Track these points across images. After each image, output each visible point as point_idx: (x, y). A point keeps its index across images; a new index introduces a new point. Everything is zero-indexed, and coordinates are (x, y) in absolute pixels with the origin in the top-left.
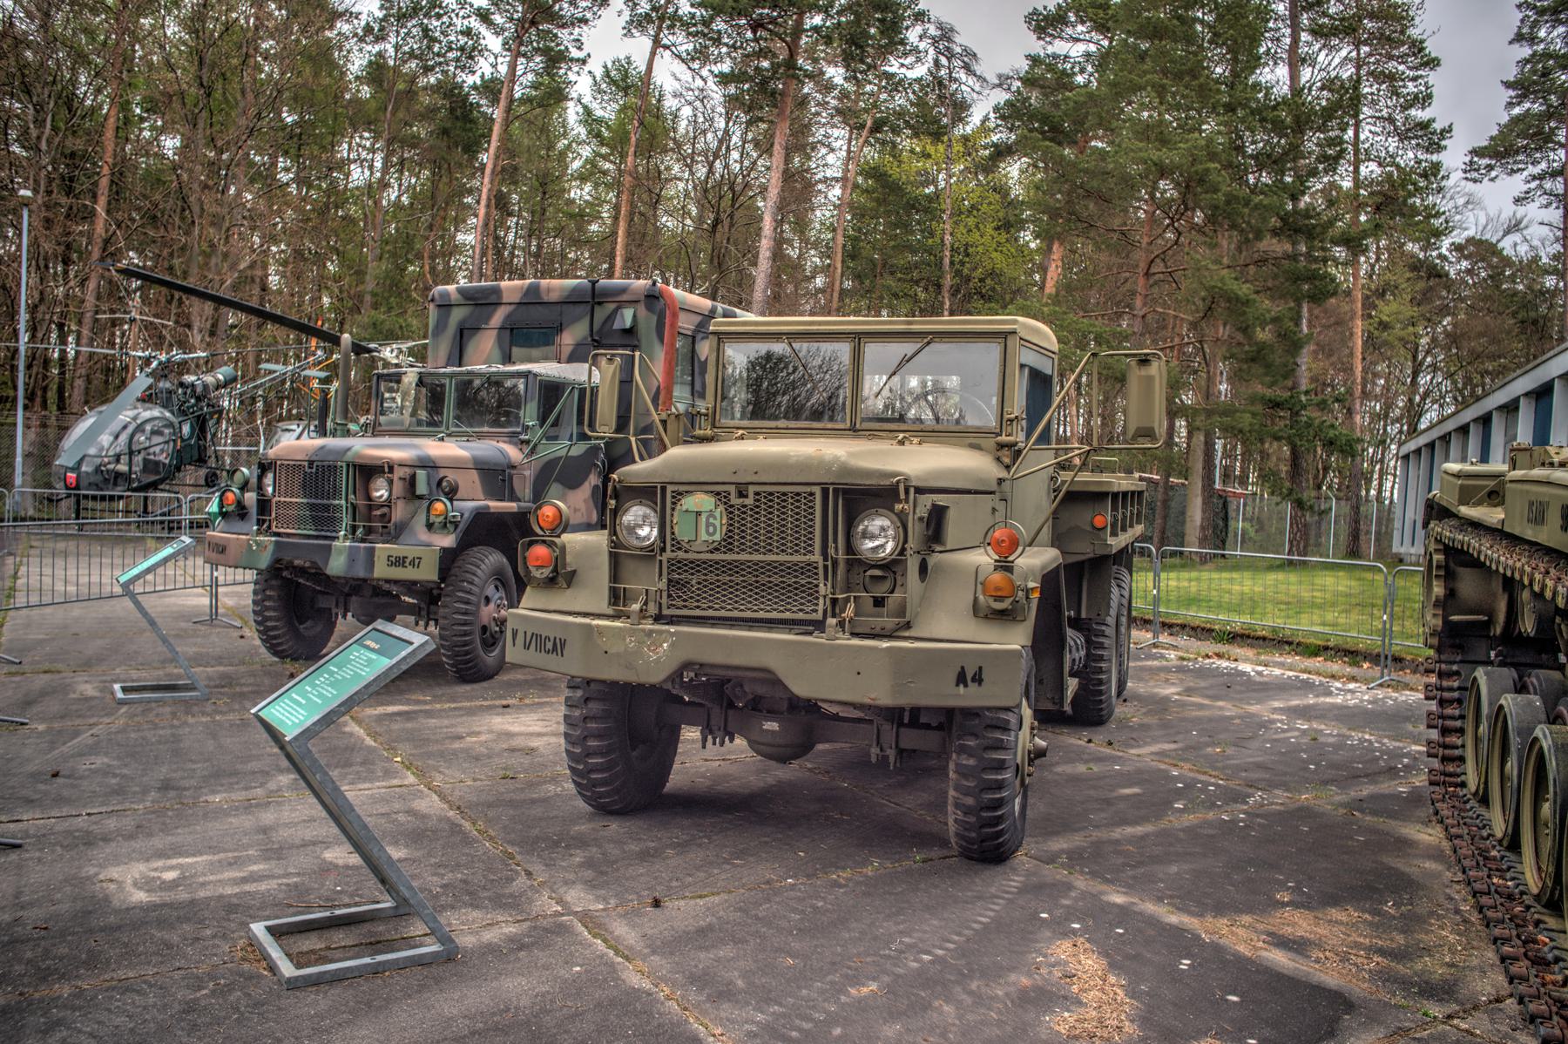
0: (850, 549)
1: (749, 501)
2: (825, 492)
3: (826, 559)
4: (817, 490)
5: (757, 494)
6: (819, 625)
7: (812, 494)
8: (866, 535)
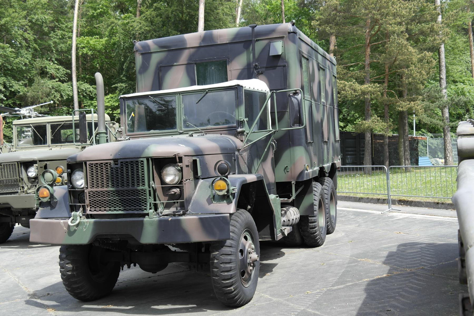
0: (163, 182)
1: (2, 167)
2: (18, 163)
3: (149, 188)
4: (16, 163)
5: (121, 162)
6: (17, 192)
7: (142, 161)
8: (30, 172)
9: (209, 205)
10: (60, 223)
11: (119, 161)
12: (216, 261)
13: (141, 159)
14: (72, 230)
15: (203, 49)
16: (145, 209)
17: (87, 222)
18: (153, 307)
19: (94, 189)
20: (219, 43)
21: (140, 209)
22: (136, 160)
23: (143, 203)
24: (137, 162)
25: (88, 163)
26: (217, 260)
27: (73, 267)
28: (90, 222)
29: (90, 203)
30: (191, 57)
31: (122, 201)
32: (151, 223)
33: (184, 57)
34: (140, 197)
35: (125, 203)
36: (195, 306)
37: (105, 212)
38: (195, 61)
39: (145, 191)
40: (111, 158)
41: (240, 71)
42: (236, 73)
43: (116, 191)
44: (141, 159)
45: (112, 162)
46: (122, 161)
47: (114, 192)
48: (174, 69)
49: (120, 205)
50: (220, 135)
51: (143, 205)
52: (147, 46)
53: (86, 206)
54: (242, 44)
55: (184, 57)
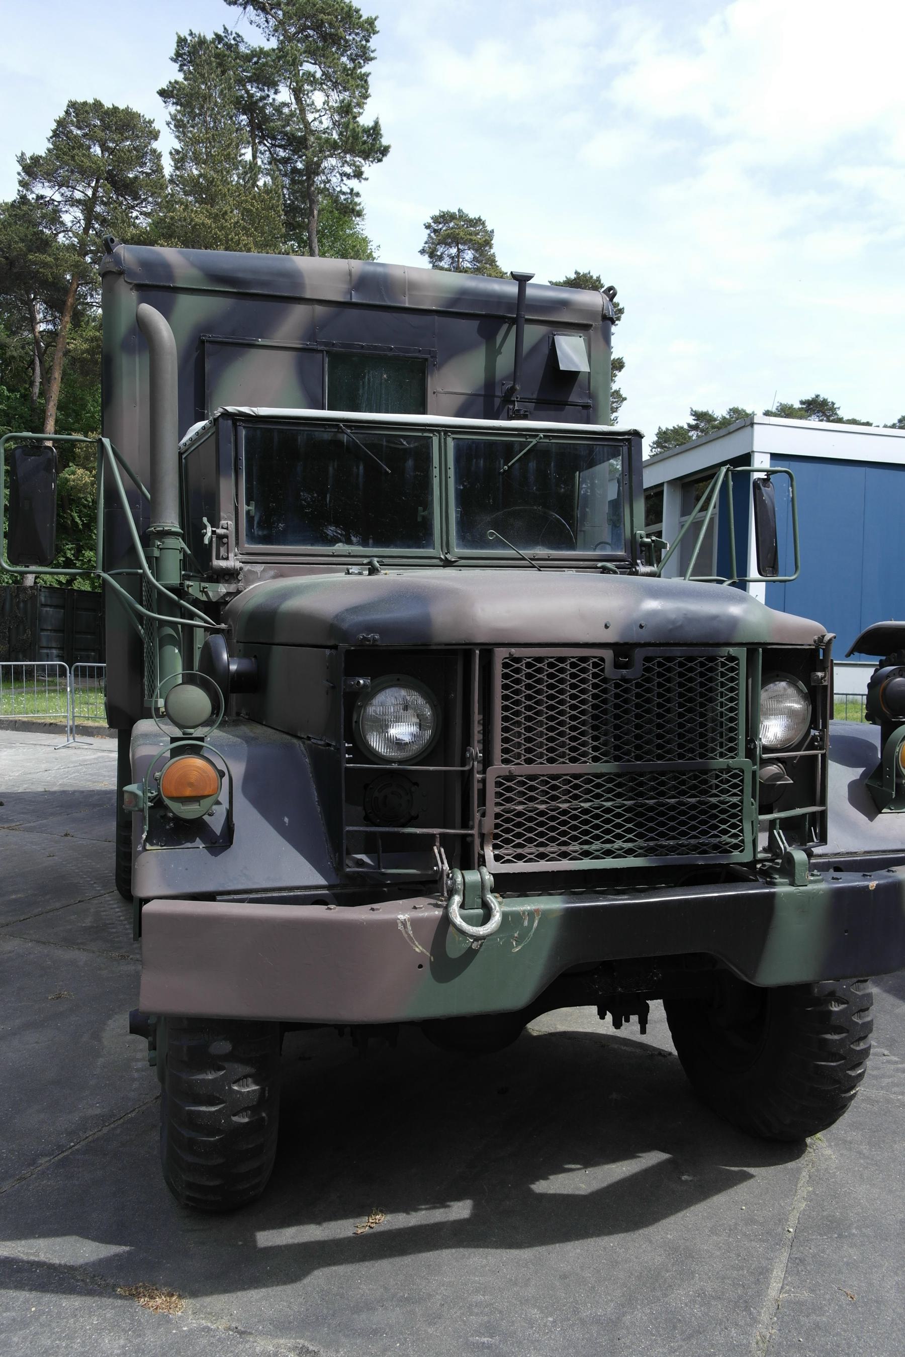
5: (648, 659)
7: (732, 659)
9: (871, 816)
10: (393, 923)
11: (639, 655)
12: (835, 1008)
13: (732, 651)
14: (454, 950)
15: (355, 312)
16: (736, 847)
17: (531, 914)
18: (541, 1187)
19: (521, 769)
20: (407, 305)
21: (716, 847)
22: (711, 651)
23: (724, 822)
24: (712, 659)
25: (500, 654)
26: (840, 1001)
27: (262, 1090)
28: (545, 914)
29: (497, 826)
30: (312, 331)
31: (640, 815)
32: (804, 903)
33: (293, 323)
34: (714, 800)
35: (646, 823)
36: (653, 1158)
37: (565, 865)
38: (326, 344)
39: (735, 776)
40: (610, 637)
41: (462, 399)
42: (446, 400)
43: (618, 775)
44: (732, 651)
45: (608, 654)
46: (650, 651)
47: (610, 781)
48: (256, 357)
49: (629, 831)
50: (365, 577)
51: (725, 832)
52: (166, 268)
53: (477, 841)
54: (475, 324)
55: (293, 323)
